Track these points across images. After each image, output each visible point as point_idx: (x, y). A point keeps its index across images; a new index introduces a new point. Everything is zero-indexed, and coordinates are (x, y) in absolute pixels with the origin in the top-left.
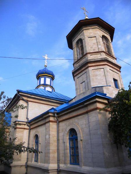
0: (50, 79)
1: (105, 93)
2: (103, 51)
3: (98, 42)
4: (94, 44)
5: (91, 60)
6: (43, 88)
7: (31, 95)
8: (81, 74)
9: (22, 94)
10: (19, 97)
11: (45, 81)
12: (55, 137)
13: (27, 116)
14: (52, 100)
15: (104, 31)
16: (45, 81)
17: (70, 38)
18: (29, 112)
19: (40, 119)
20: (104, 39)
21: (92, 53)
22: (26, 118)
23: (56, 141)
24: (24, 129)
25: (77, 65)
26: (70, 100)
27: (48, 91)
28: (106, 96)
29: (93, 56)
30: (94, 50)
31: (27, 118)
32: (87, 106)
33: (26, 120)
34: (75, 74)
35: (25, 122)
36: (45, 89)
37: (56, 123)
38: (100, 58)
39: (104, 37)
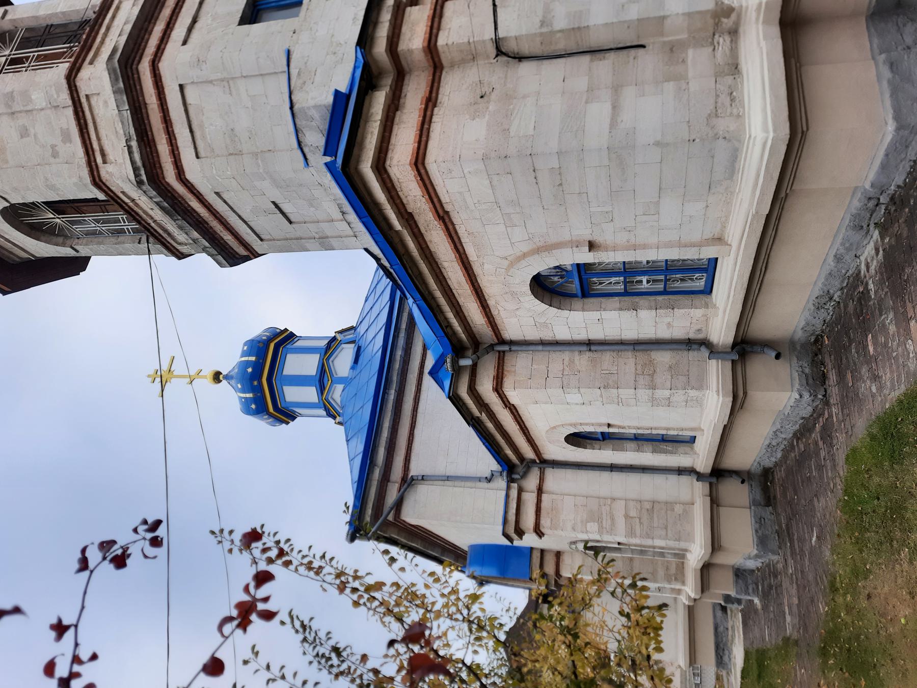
0: (289, 356)
1: (330, 99)
4: (24, 133)
5: (133, 162)
6: (339, 388)
7: (373, 464)
8: (233, 220)
9: (369, 511)
10: (386, 523)
11: (300, 381)
12: (577, 362)
13: (480, 479)
14: (399, 353)
16: (300, 381)
18: (461, 472)
19: (490, 425)
22: (491, 485)
23: (595, 355)
24: (540, 491)
25: (181, 237)
26: (386, 281)
27: (352, 368)
28: (348, 96)
30: (66, 138)
32: (408, 218)
33: (501, 483)
34: (232, 252)
35: (508, 488)
36: (341, 380)
37: (508, 357)
38: (112, 104)
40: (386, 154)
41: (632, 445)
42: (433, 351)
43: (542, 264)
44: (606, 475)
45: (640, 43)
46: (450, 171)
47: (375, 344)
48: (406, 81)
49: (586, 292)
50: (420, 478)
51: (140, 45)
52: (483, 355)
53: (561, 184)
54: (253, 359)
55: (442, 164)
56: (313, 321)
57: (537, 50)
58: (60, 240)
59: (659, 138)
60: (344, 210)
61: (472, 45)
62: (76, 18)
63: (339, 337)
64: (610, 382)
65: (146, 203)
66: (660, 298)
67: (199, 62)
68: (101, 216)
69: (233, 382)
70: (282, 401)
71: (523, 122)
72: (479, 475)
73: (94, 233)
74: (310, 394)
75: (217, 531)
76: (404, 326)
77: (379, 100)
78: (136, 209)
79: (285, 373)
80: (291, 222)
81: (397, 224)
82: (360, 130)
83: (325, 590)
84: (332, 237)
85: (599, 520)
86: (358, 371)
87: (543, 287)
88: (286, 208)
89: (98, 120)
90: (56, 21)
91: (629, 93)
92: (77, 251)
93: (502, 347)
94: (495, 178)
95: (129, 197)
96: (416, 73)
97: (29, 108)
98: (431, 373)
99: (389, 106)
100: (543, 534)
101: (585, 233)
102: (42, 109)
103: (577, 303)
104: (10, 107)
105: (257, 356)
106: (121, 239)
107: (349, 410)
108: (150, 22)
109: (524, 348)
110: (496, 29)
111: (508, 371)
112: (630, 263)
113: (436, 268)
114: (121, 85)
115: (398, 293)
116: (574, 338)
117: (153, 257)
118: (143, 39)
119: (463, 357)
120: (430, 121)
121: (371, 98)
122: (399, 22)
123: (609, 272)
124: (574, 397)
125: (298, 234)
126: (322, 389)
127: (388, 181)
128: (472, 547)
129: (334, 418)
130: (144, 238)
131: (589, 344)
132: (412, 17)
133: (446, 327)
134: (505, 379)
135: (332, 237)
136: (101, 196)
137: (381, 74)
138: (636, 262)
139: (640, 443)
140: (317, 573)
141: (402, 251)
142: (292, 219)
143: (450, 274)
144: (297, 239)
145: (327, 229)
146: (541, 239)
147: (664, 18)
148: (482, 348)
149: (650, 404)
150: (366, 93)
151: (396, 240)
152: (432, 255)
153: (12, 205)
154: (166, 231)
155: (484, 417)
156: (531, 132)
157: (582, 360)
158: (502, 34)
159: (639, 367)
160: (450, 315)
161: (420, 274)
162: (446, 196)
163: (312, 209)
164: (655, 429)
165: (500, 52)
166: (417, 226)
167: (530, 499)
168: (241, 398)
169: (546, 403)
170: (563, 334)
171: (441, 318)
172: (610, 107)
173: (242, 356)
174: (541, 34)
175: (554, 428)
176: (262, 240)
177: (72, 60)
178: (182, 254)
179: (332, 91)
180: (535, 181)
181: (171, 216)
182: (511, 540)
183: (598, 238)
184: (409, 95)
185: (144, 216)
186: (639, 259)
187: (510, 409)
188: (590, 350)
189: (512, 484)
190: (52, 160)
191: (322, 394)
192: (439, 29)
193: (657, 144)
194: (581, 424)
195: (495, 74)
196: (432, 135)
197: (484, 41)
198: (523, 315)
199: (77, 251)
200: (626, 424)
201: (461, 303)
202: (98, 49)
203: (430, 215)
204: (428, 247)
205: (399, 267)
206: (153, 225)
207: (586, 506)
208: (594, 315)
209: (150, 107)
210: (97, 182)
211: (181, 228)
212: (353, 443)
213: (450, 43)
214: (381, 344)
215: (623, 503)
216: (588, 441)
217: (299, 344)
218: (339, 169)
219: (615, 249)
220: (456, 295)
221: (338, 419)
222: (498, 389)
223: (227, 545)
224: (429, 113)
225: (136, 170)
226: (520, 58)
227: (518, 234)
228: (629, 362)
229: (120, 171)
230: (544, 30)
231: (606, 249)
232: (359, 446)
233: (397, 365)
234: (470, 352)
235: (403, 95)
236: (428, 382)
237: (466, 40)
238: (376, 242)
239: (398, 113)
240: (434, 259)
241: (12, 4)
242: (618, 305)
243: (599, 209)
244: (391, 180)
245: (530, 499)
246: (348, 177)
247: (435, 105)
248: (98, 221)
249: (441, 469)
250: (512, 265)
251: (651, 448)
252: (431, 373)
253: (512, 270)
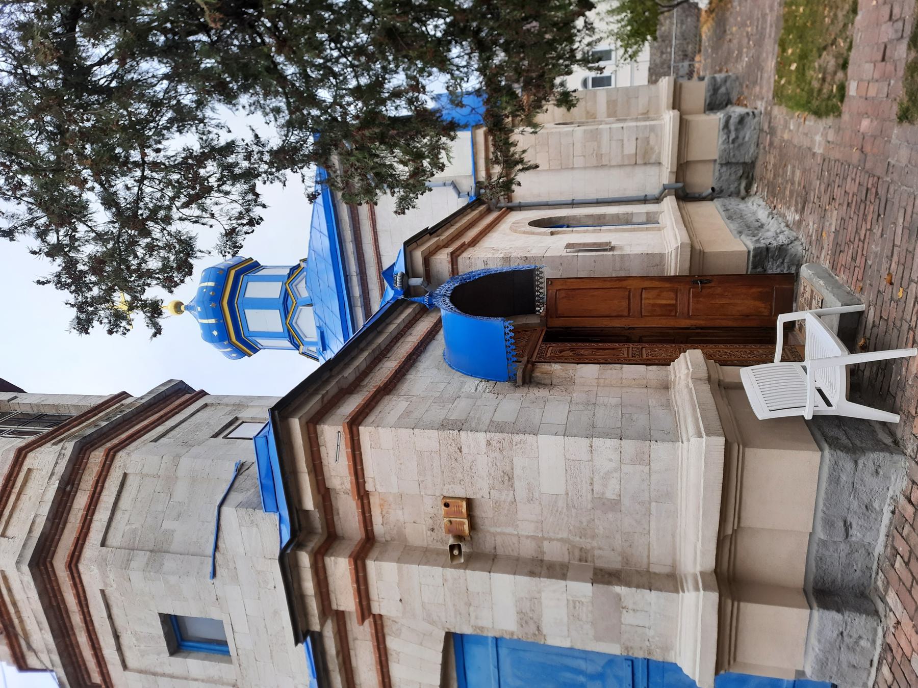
11: (262, 304)
16: (262, 304)
51: (78, 662)
63: (303, 265)
70: (245, 330)
79: (247, 296)
108: (69, 635)
118: (75, 655)
129: (297, 347)
191: (286, 318)
202: (24, 630)
209: (69, 526)
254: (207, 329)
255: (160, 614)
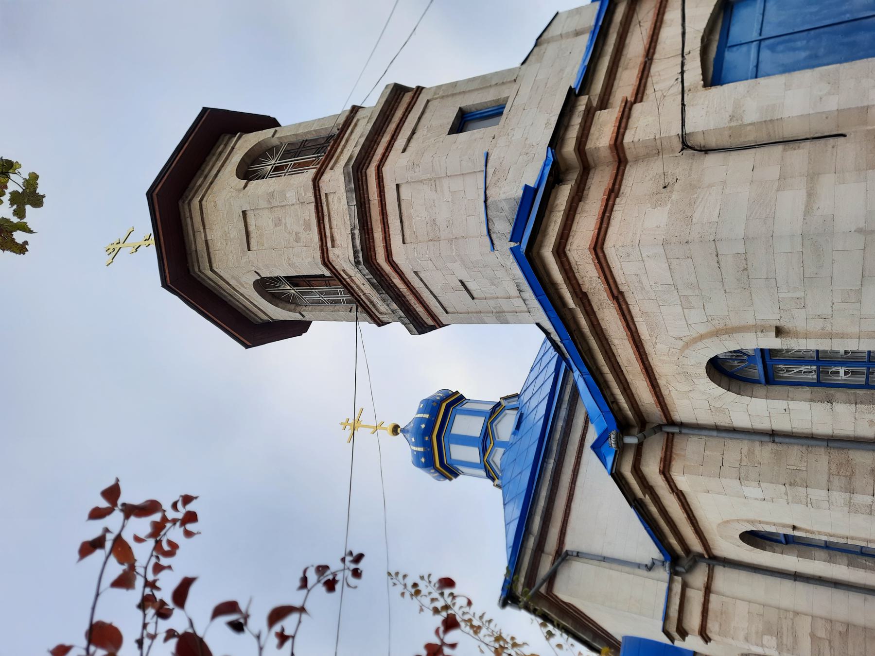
1: (520, 193)
2: (311, 183)
3: (269, 202)
4: (278, 223)
5: (354, 246)
6: (500, 451)
10: (538, 596)
11: (465, 440)
13: (639, 566)
14: (560, 424)
15: (219, 164)
16: (465, 440)
17: (250, 330)
19: (653, 509)
20: (255, 167)
21: (321, 239)
22: (651, 574)
24: (708, 590)
25: (382, 307)
26: (552, 352)
27: (514, 433)
28: (536, 190)
29: (336, 235)
30: (307, 227)
31: (650, 568)
32: (582, 298)
33: (663, 574)
34: (421, 322)
35: (671, 581)
36: (503, 444)
39: (248, 171)
40: (567, 240)
41: (823, 554)
42: (597, 426)
43: (720, 348)
44: (788, 584)
45: (840, 132)
46: (628, 255)
47: (537, 413)
48: (591, 175)
49: (771, 379)
50: (575, 554)
52: (650, 435)
53: (746, 269)
54: (427, 416)
55: (621, 249)
56: (482, 388)
57: (725, 142)
58: (293, 306)
59: (862, 225)
60: (522, 288)
61: (658, 142)
62: (324, 134)
63: (504, 403)
64: (798, 480)
65: (360, 279)
66: (861, 392)
67: (414, 165)
68: (325, 289)
69: (408, 436)
71: (707, 210)
72: (638, 561)
73: (318, 303)
74: (472, 454)
75: (393, 574)
76: (567, 398)
77: (564, 193)
78: (351, 284)
79: (453, 432)
80: (473, 298)
81: (571, 303)
82: (545, 219)
83: (482, 651)
84: (509, 312)
85: (779, 635)
86: (519, 437)
87: (721, 370)
88: (470, 285)
89: (332, 213)
90: (309, 137)
91: (827, 181)
92: (303, 316)
93: (672, 429)
94: (674, 262)
95: (347, 275)
96: (601, 168)
97: (283, 204)
98: (594, 447)
99: (573, 198)
100: (710, 640)
101: (773, 319)
102: (292, 205)
103: (761, 390)
104: (270, 202)
105: (430, 414)
106: (337, 307)
107: (508, 475)
109: (696, 432)
110: (683, 125)
111: (677, 455)
112: (825, 352)
113: (605, 345)
114: (353, 186)
115: (564, 364)
116: (754, 427)
117: (360, 323)
119: (629, 434)
120: (612, 210)
121: (557, 194)
122: (588, 124)
123: (800, 359)
124: (752, 491)
125: (479, 308)
126: (484, 451)
127: (566, 263)
128: (626, 638)
129: (493, 480)
130: (354, 307)
131: (773, 435)
132: (601, 120)
133: (612, 403)
134: (673, 463)
135: (509, 312)
136: (327, 273)
137: (568, 169)
138: (833, 352)
139: (831, 552)
140: (476, 632)
141: (573, 327)
142: (475, 296)
143: (619, 351)
144: (477, 313)
145: (505, 305)
146: (721, 322)
147: (868, 107)
148: (648, 427)
149: (846, 509)
150: (553, 187)
151: (569, 317)
152: (602, 332)
153: (262, 278)
154: (372, 302)
155: (647, 499)
156: (715, 219)
157: (764, 452)
158: (688, 129)
159: (834, 467)
160: (617, 392)
161: (590, 350)
162: (622, 278)
163: (493, 287)
164: (852, 538)
165: (685, 146)
166: (590, 305)
167: (696, 597)
168: (413, 451)
169: (719, 493)
170: (741, 420)
171: (608, 394)
172: (805, 194)
173: (418, 413)
174: (730, 128)
175: (728, 522)
176: (447, 312)
177: (318, 166)
178: (382, 322)
179: (523, 185)
180: (717, 265)
181: (378, 291)
182: (672, 639)
183: (785, 324)
184: (592, 188)
185: (357, 290)
186: (835, 348)
187: (677, 494)
188: (774, 442)
189: (676, 577)
190: (295, 244)
191: (484, 455)
192: (626, 128)
193: (859, 231)
194: (760, 522)
195: (680, 167)
196: (612, 222)
197: (670, 137)
198: (695, 397)
199: (303, 316)
200: (815, 528)
201: (629, 380)
202: (338, 157)
203: (605, 294)
204: (599, 324)
205: (569, 341)
206: (362, 297)
207: (762, 615)
208: (778, 405)
209: (372, 203)
210: (326, 262)
211: (384, 300)
212: (510, 507)
213: (636, 140)
214: (544, 412)
215: (809, 619)
216: (768, 542)
217: (467, 406)
218: (523, 254)
219: (806, 336)
220: (625, 372)
221: (497, 482)
222: (665, 472)
223: (400, 588)
224: (611, 203)
225: (355, 252)
226: (706, 150)
227: (696, 316)
228: (821, 460)
229: (343, 255)
230: (733, 124)
231: (796, 335)
232: (516, 511)
233: (558, 435)
234: (636, 431)
235: (587, 187)
236: (590, 457)
237: (652, 137)
238: (549, 318)
239: (581, 203)
240: (604, 336)
241: (280, 126)
242: (809, 396)
243: (790, 295)
244: (569, 263)
245: (696, 597)
246: (530, 262)
247: (617, 196)
248: (321, 293)
249: (597, 546)
250: (687, 346)
251: (845, 560)
252: (594, 447)
253: (687, 351)
254: (417, 456)
255: (449, 134)
